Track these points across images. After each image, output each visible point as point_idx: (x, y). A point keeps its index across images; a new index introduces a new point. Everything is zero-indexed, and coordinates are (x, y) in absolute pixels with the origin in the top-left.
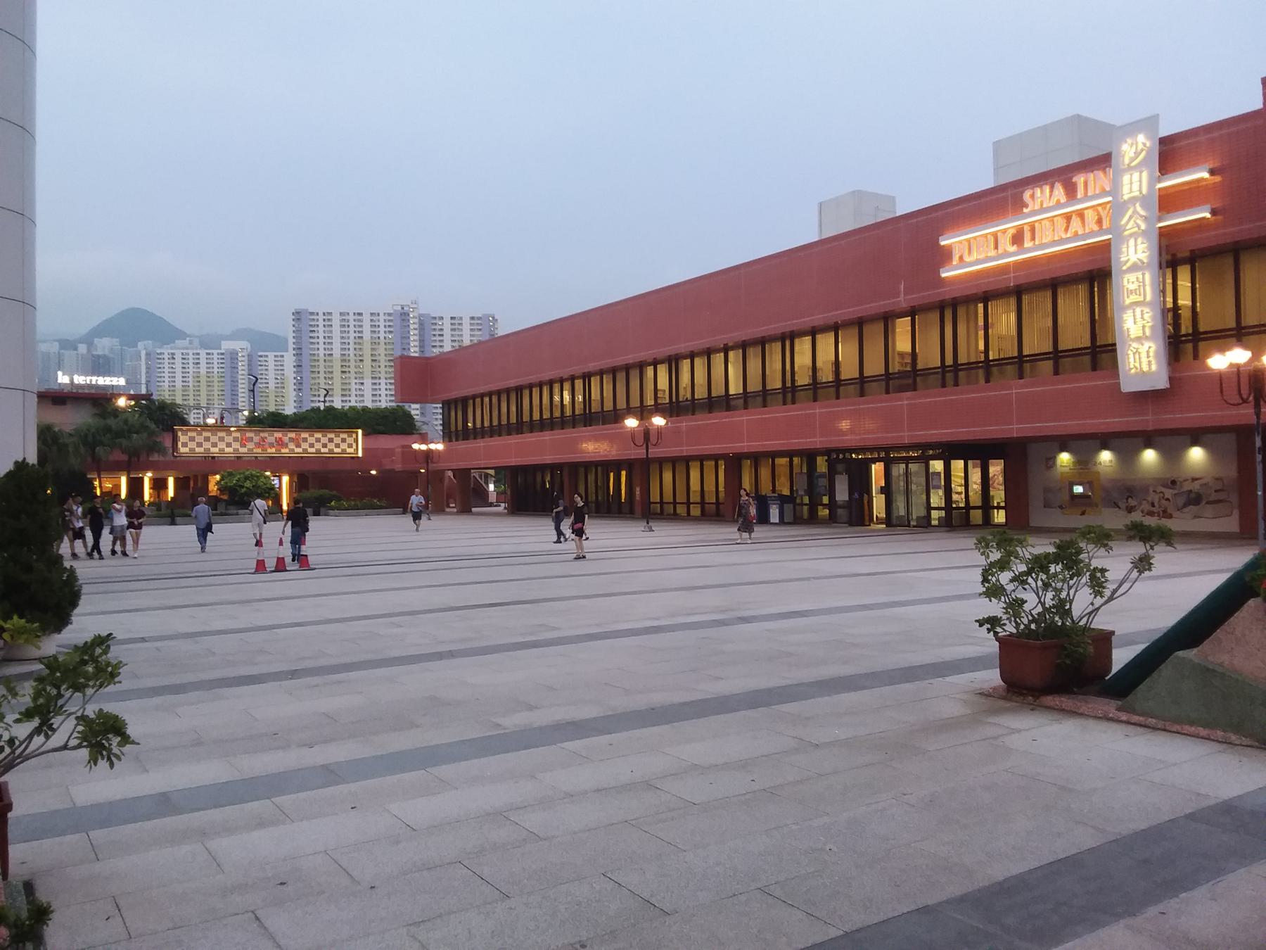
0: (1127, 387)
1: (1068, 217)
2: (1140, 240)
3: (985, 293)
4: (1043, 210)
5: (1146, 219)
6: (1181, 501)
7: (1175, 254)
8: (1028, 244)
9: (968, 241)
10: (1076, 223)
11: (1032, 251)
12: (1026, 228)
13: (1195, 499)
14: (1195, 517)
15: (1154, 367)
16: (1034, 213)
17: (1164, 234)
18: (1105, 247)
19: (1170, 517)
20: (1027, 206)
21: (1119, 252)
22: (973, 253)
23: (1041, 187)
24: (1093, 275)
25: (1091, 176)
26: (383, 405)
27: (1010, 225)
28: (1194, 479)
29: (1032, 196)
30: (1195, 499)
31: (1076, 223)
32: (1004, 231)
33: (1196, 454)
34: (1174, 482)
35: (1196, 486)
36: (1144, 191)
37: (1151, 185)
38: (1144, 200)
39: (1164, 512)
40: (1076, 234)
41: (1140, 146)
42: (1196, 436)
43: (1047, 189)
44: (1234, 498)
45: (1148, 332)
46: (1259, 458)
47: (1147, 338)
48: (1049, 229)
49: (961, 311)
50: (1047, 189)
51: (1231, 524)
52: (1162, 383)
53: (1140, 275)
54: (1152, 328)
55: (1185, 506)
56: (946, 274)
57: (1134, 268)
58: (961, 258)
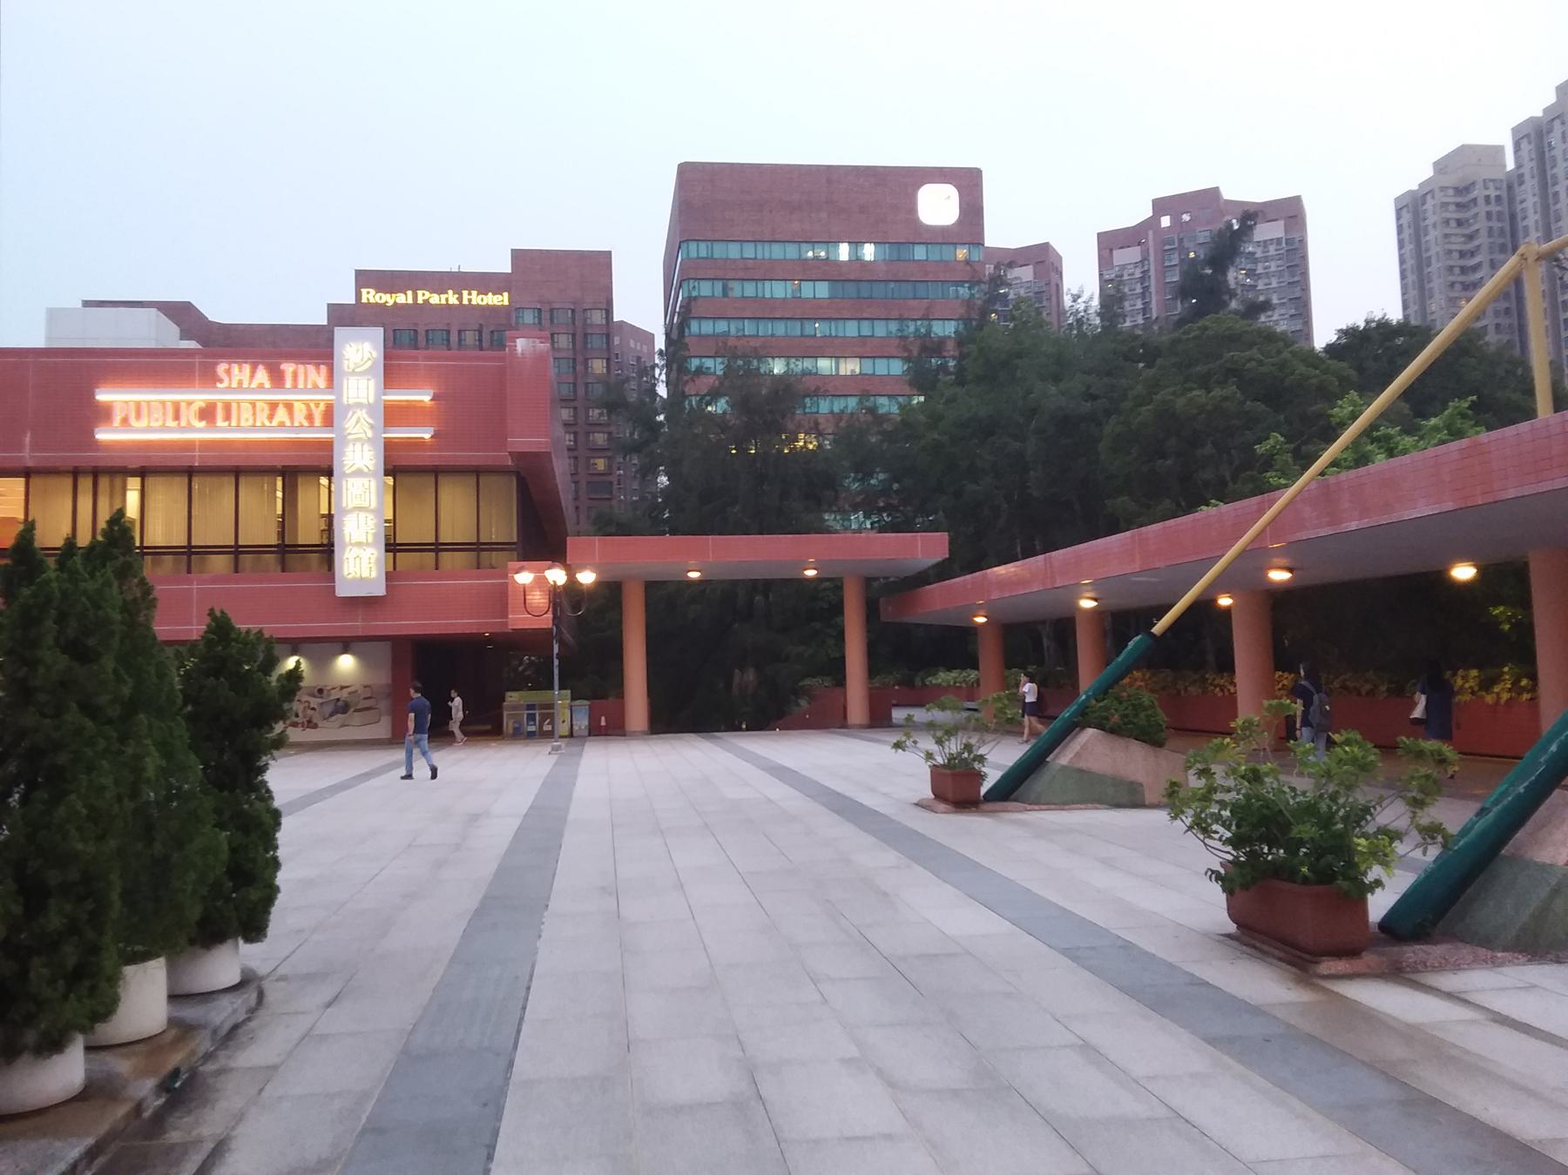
0: (342, 591)
1: (273, 406)
2: (366, 447)
3: (150, 467)
4: (240, 388)
5: (372, 427)
6: (329, 709)
7: (400, 468)
8: (220, 423)
9: (138, 405)
10: (281, 414)
11: (222, 432)
12: (219, 406)
13: (342, 708)
14: (343, 726)
15: (374, 574)
16: (229, 389)
17: (389, 445)
18: (327, 446)
19: (315, 726)
20: (221, 381)
21: (343, 454)
22: (137, 417)
23: (240, 364)
24: (306, 467)
25: (301, 368)
26: (365, 574)
27: (200, 398)
28: (342, 688)
29: (228, 372)
30: (342, 708)
31: (281, 414)
32: (190, 403)
33: (346, 663)
34: (321, 691)
35: (344, 694)
36: (371, 400)
37: (377, 398)
38: (370, 408)
39: (309, 722)
40: (282, 425)
41: (367, 355)
42: (346, 644)
43: (247, 368)
44: (384, 705)
45: (370, 539)
46: (556, 662)
47: (368, 544)
48: (248, 409)
49: (104, 482)
50: (247, 368)
51: (382, 729)
52: (380, 590)
53: (365, 480)
54: (375, 535)
55: (331, 715)
56: (102, 435)
57: (358, 473)
58: (125, 421)
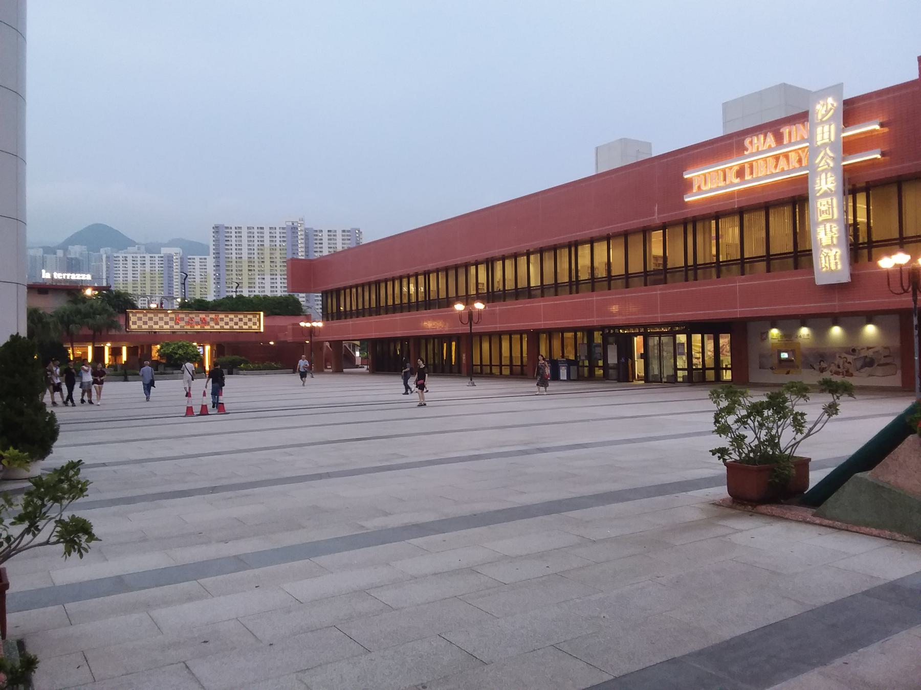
0: (820, 281)
1: (777, 158)
2: (829, 174)
3: (717, 213)
4: (759, 152)
5: (834, 159)
6: (859, 364)
7: (854, 184)
8: (748, 177)
9: (705, 175)
10: (782, 162)
11: (750, 182)
12: (747, 166)
13: (869, 363)
14: (870, 375)
15: (839, 267)
16: (752, 155)
17: (847, 170)
18: (804, 180)
19: (851, 375)
20: (747, 150)
21: (814, 183)
22: (708, 184)
23: (757, 136)
24: (795, 200)
25: (794, 128)
26: (279, 294)
27: (735, 164)
28: (869, 348)
29: (751, 143)
30: (869, 363)
31: (782, 162)
32: (731, 168)
33: (870, 330)
34: (854, 350)
35: (870, 353)
36: (833, 139)
37: (837, 135)
38: (832, 145)
39: (847, 372)
40: (783, 170)
41: (830, 106)
42: (870, 317)
43: (762, 137)
44: (898, 362)
45: (835, 241)
46: (916, 332)
47: (834, 246)
48: (763, 166)
49: (699, 226)
50: (762, 137)
51: (895, 380)
52: (845, 278)
53: (829, 199)
54: (838, 238)
55: (862, 367)
56: (688, 199)
57: (825, 195)
58: (699, 188)
